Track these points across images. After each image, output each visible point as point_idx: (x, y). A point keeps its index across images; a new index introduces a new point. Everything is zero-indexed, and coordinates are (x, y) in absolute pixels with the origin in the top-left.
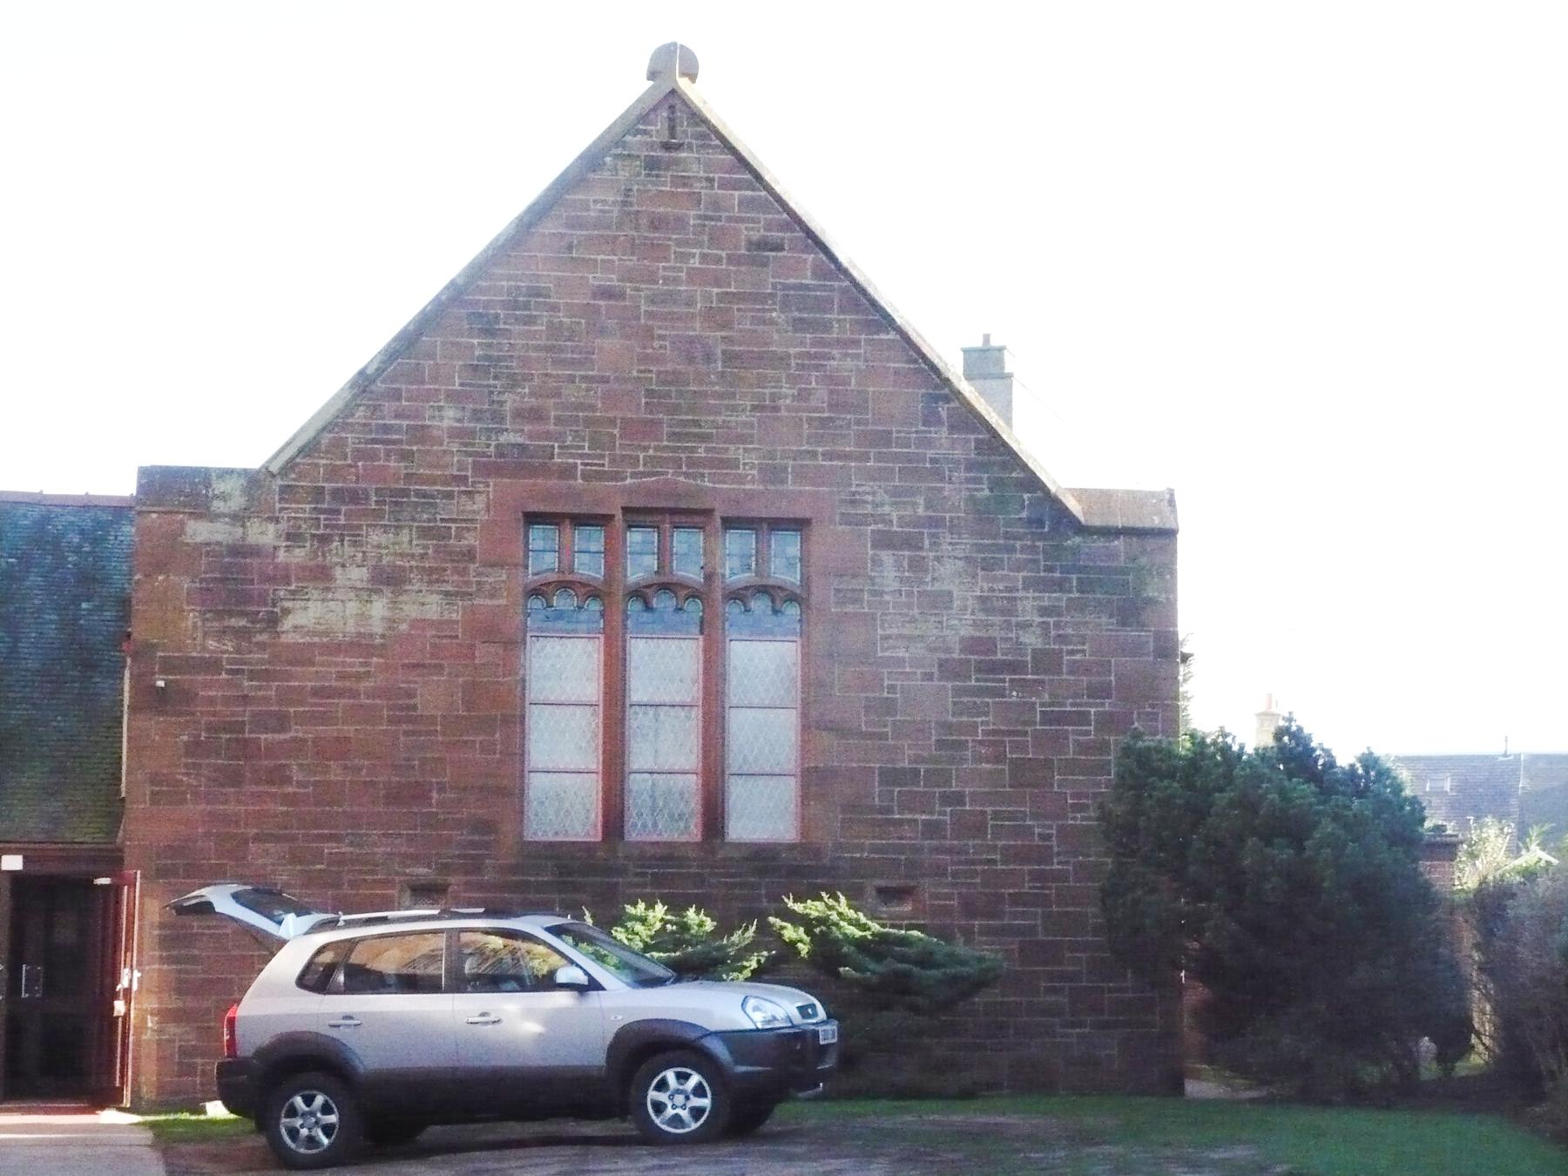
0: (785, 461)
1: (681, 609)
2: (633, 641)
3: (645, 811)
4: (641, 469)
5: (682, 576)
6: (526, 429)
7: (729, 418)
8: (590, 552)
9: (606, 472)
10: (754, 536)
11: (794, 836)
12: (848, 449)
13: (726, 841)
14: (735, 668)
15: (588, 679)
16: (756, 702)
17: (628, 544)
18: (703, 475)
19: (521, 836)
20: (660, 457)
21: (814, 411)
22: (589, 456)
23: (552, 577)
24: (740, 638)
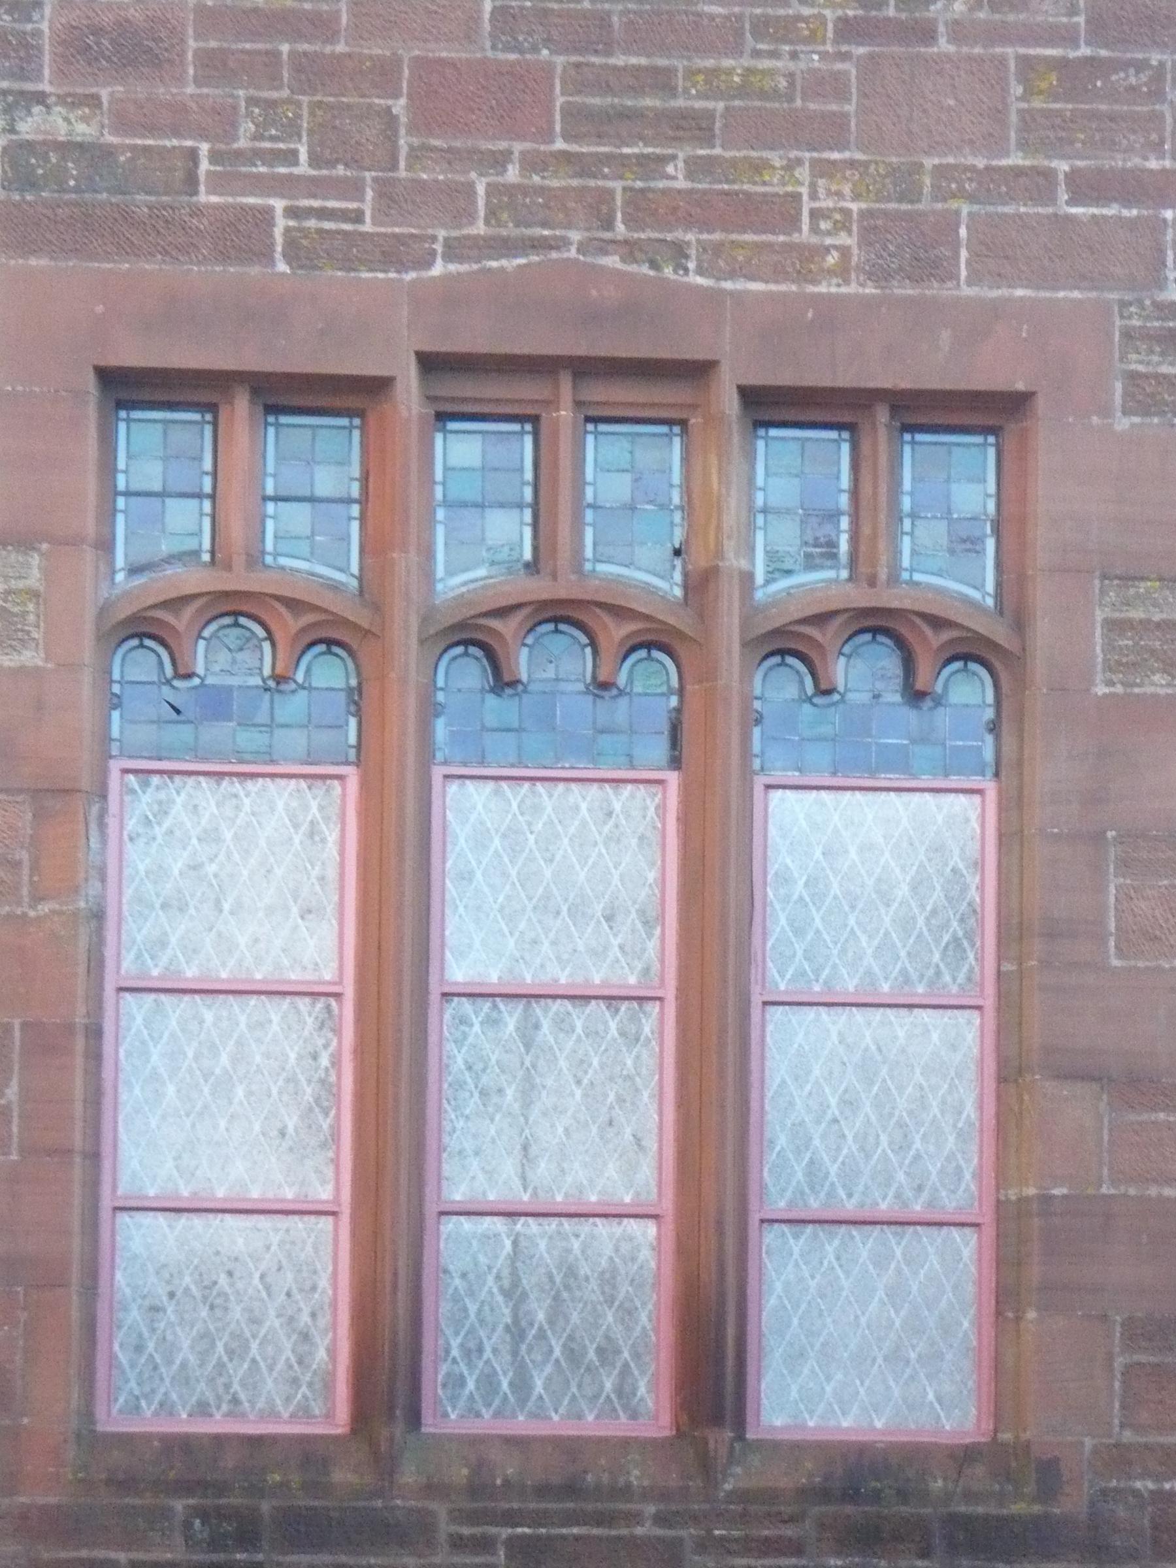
0: (953, 205)
1: (605, 686)
2: (453, 788)
3: (494, 1341)
4: (480, 228)
5: (618, 580)
6: (104, 94)
7: (765, 64)
8: (312, 499)
9: (364, 236)
10: (846, 448)
11: (970, 1424)
12: (1153, 164)
13: (750, 1435)
14: (785, 879)
15: (305, 913)
16: (849, 984)
17: (439, 475)
18: (679, 252)
19: (88, 1415)
20: (541, 190)
21: (1038, 41)
22: (314, 186)
23: (193, 579)
24: (793, 777)
